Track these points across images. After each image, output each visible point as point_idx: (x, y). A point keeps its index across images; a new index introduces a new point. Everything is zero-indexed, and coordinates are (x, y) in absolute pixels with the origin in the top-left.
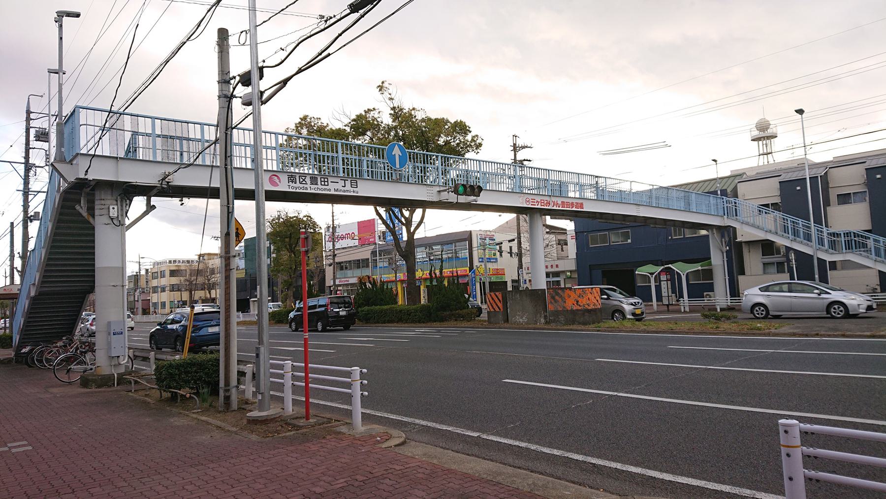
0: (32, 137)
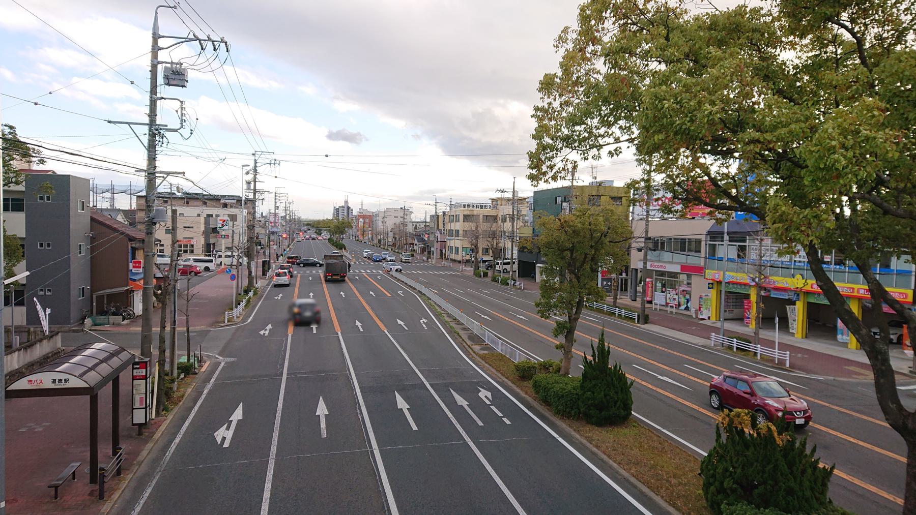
0: (160, 80)
